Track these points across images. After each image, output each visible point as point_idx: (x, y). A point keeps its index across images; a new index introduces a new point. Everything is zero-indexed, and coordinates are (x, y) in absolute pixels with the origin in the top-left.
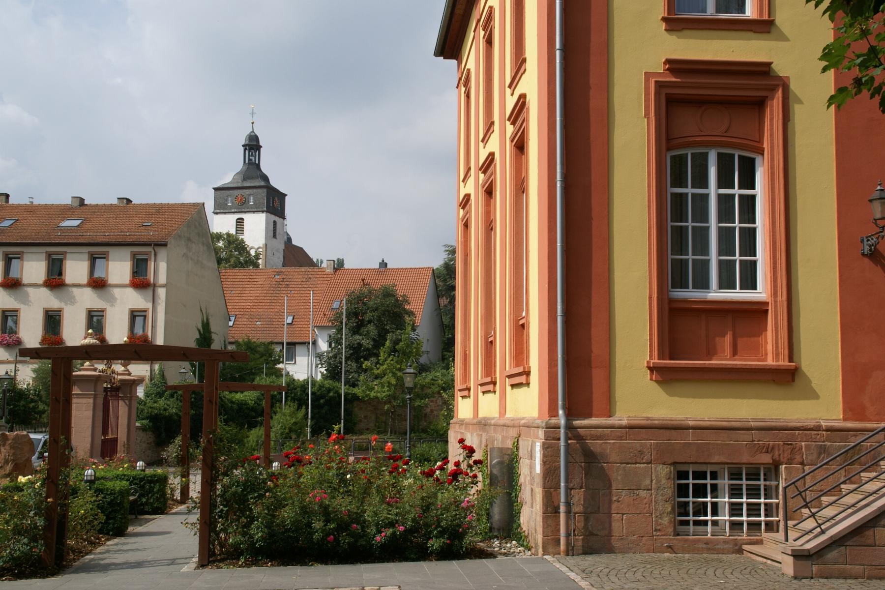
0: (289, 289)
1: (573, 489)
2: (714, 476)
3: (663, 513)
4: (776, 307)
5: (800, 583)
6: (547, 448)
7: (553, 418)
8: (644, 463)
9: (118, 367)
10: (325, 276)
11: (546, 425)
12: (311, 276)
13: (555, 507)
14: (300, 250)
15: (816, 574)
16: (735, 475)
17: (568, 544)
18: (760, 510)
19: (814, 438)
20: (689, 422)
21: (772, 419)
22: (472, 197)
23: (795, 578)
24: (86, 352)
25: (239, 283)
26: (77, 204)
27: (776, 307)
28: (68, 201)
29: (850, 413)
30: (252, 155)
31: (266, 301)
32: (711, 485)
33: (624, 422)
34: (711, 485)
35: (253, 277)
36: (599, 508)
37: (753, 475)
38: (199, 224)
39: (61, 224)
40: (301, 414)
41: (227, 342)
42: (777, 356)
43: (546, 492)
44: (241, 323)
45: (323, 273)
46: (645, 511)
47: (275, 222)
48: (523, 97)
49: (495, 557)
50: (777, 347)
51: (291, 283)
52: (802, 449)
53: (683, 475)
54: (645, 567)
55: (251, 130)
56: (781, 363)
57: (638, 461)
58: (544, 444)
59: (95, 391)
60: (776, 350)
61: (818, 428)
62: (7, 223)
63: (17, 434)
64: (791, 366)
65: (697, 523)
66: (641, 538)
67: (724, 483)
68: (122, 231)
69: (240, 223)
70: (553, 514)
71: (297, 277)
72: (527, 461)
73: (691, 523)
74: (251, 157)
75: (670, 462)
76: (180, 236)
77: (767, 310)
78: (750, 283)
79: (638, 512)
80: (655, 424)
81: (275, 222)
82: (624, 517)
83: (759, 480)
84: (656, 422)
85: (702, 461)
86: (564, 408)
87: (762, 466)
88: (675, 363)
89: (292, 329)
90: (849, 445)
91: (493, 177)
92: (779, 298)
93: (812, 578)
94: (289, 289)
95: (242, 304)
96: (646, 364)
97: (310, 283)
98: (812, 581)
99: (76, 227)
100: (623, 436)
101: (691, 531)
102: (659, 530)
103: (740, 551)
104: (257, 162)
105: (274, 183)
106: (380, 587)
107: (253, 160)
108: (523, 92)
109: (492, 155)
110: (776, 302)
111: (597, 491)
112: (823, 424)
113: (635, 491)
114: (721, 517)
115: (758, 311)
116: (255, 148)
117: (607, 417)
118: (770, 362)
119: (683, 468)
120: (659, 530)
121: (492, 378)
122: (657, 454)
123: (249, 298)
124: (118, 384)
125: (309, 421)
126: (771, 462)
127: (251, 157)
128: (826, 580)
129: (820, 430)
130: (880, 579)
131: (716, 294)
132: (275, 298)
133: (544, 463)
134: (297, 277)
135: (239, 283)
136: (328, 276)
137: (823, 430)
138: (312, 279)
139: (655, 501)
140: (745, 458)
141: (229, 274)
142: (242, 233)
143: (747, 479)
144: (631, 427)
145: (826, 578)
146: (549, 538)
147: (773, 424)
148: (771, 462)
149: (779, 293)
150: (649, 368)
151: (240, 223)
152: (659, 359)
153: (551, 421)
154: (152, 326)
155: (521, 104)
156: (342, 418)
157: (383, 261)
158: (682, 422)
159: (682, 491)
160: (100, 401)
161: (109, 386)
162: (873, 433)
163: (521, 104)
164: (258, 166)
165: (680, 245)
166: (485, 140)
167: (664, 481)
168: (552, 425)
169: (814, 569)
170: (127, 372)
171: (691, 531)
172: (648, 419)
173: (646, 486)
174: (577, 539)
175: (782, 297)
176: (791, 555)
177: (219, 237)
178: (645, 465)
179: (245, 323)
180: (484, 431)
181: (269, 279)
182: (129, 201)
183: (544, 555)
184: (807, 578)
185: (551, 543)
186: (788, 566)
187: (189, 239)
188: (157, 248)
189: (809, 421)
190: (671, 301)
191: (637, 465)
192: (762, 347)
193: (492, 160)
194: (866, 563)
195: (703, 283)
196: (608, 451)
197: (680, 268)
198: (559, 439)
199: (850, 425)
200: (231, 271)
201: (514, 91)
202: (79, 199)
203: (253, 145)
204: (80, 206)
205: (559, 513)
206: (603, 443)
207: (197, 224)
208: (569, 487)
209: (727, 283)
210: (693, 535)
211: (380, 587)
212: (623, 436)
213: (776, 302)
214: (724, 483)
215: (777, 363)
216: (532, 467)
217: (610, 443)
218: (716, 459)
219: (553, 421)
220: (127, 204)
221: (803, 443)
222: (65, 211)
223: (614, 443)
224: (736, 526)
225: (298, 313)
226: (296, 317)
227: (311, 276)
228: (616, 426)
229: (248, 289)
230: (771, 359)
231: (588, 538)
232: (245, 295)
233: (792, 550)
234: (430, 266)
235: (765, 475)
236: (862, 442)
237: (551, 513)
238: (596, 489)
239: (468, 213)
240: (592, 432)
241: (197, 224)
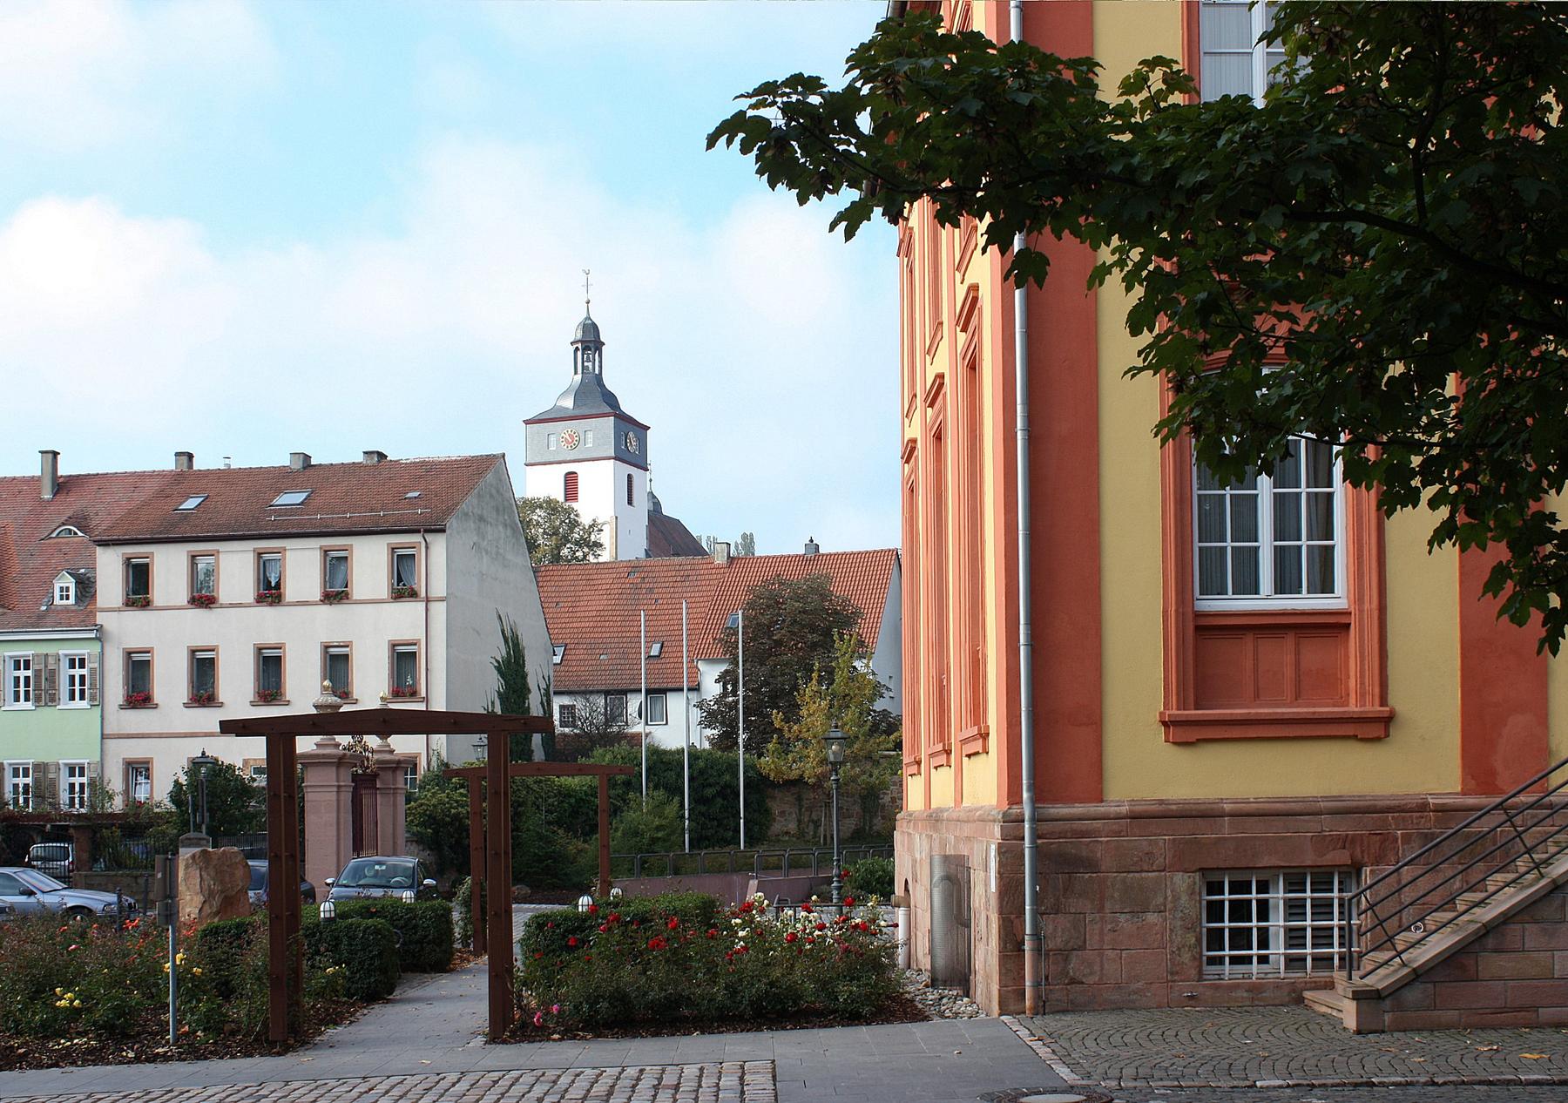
0: (653, 596)
1: (1044, 914)
2: (1263, 887)
3: (1183, 946)
4: (1361, 620)
5: (1363, 1040)
6: (1005, 852)
7: (1014, 807)
8: (1154, 871)
9: (372, 741)
10: (714, 571)
11: (1003, 817)
12: (690, 572)
13: (1019, 943)
14: (676, 524)
15: (1389, 1026)
16: (1295, 884)
17: (1037, 996)
18: (1305, 937)
19: (1417, 823)
20: (1225, 805)
21: (1354, 796)
22: (919, 445)
23: (1359, 1032)
24: (314, 724)
25: (568, 589)
26: (298, 465)
27: (1361, 620)
28: (283, 460)
29: (1473, 781)
30: (588, 361)
31: (614, 619)
32: (1258, 901)
33: (1124, 809)
34: (1258, 901)
35: (591, 577)
36: (1085, 942)
37: (1322, 883)
38: (498, 491)
39: (275, 502)
40: (671, 810)
41: (552, 690)
42: (1362, 696)
43: (1004, 919)
44: (574, 657)
45: (709, 566)
46: (1155, 945)
47: (630, 477)
48: (974, 288)
49: (926, 1018)
50: (1362, 683)
51: (655, 585)
52: (1397, 842)
53: (1215, 888)
54: (1145, 1026)
55: (585, 315)
56: (1368, 708)
57: (1146, 868)
58: (1000, 846)
59: (338, 781)
60: (1360, 688)
61: (1423, 807)
62: (191, 503)
63: (224, 851)
64: (1383, 711)
65: (1235, 960)
66: (1148, 986)
67: (1278, 896)
68: (372, 510)
69: (571, 481)
70: (1015, 953)
71: (666, 574)
72: (982, 874)
73: (1255, 960)
74: (586, 364)
75: (1194, 868)
76: (466, 514)
77: (1350, 624)
78: (1324, 584)
79: (1146, 947)
80: (1172, 810)
81: (630, 477)
82: (1123, 955)
83: (1331, 891)
84: (1174, 807)
85: (1243, 864)
86: (1029, 790)
87: (1337, 869)
88: (1203, 714)
89: (660, 666)
90: (1480, 832)
91: (941, 417)
92: (1366, 606)
93: (1383, 1032)
94: (653, 596)
95: (575, 625)
96: (1158, 719)
97: (687, 584)
98: (1383, 1036)
99: (299, 504)
100: (1122, 831)
101: (1227, 972)
102: (1177, 973)
103: (1300, 1000)
104: (597, 372)
105: (626, 407)
106: (745, 1062)
107: (591, 367)
108: (973, 281)
109: (941, 376)
110: (1361, 611)
111: (1082, 916)
112: (1431, 801)
113: (1141, 915)
114: (1273, 949)
115: (1332, 627)
116: (591, 345)
117: (1097, 803)
118: (1353, 708)
119: (1214, 878)
120: (1177, 973)
121: (944, 745)
122: (1174, 857)
123: (587, 614)
124: (373, 767)
125: (687, 822)
126: (1349, 862)
127: (586, 364)
128: (1403, 1033)
129: (1425, 811)
130: (1482, 1029)
131: (1267, 600)
132: (630, 613)
133: (1000, 875)
134: (666, 574)
135: (568, 589)
136: (718, 571)
137: (1431, 811)
138: (691, 578)
139: (1170, 929)
140: (1309, 859)
141: (552, 573)
142: (575, 499)
143: (1312, 891)
144: (1134, 817)
145: (1404, 1031)
146: (1010, 988)
147: (1355, 804)
148: (1349, 862)
149: (1367, 598)
150: (1165, 724)
151: (571, 481)
152: (1178, 709)
153: (1011, 811)
154: (427, 669)
155: (972, 301)
156: (742, 816)
157: (812, 541)
158: (1214, 806)
159: (1215, 911)
160: (347, 797)
161: (360, 772)
162: (1480, 813)
163: (972, 301)
164: (599, 379)
165: (1212, 529)
166: (931, 351)
167: (1184, 899)
168: (1013, 818)
169: (1386, 1018)
170: (387, 749)
171: (1227, 972)
172: (1161, 802)
173: (1157, 905)
174: (1051, 990)
175: (1371, 604)
176: (1353, 999)
177: (533, 505)
178: (1157, 873)
179: (582, 657)
180: (936, 830)
181: (619, 581)
182: (381, 456)
183: (1000, 1015)
184: (1375, 1032)
185: (1010, 1001)
186: (1349, 1015)
187: (481, 519)
188: (429, 537)
189: (1409, 797)
190: (1199, 615)
191: (1143, 874)
192: (1341, 684)
193: (941, 385)
194: (1463, 1007)
195: (1249, 585)
196: (1099, 855)
197: (1211, 561)
198: (1023, 839)
199: (1471, 801)
200: (555, 568)
201: (964, 276)
202: (302, 456)
203: (590, 342)
204: (304, 468)
205: (1024, 950)
206: (1091, 841)
207: (494, 491)
208: (1039, 911)
209: (1285, 584)
210: (1230, 979)
211: (745, 1062)
212: (1122, 831)
213: (1361, 611)
214: (1278, 896)
215: (1362, 709)
216: (987, 885)
217: (1101, 842)
218: (1265, 861)
219: (1015, 810)
220: (379, 461)
221: (1399, 832)
222: (279, 478)
223: (1108, 841)
224: (1294, 962)
225: (669, 638)
226: (666, 644)
227: (690, 572)
228: (1112, 816)
229: (585, 598)
230: (1354, 702)
231: (1069, 987)
232: (579, 609)
233: (1353, 992)
234: (891, 548)
235: (1340, 883)
236: (1465, 827)
237: (1012, 951)
238: (1080, 913)
239: (914, 471)
240: (1074, 826)
241: (494, 491)
